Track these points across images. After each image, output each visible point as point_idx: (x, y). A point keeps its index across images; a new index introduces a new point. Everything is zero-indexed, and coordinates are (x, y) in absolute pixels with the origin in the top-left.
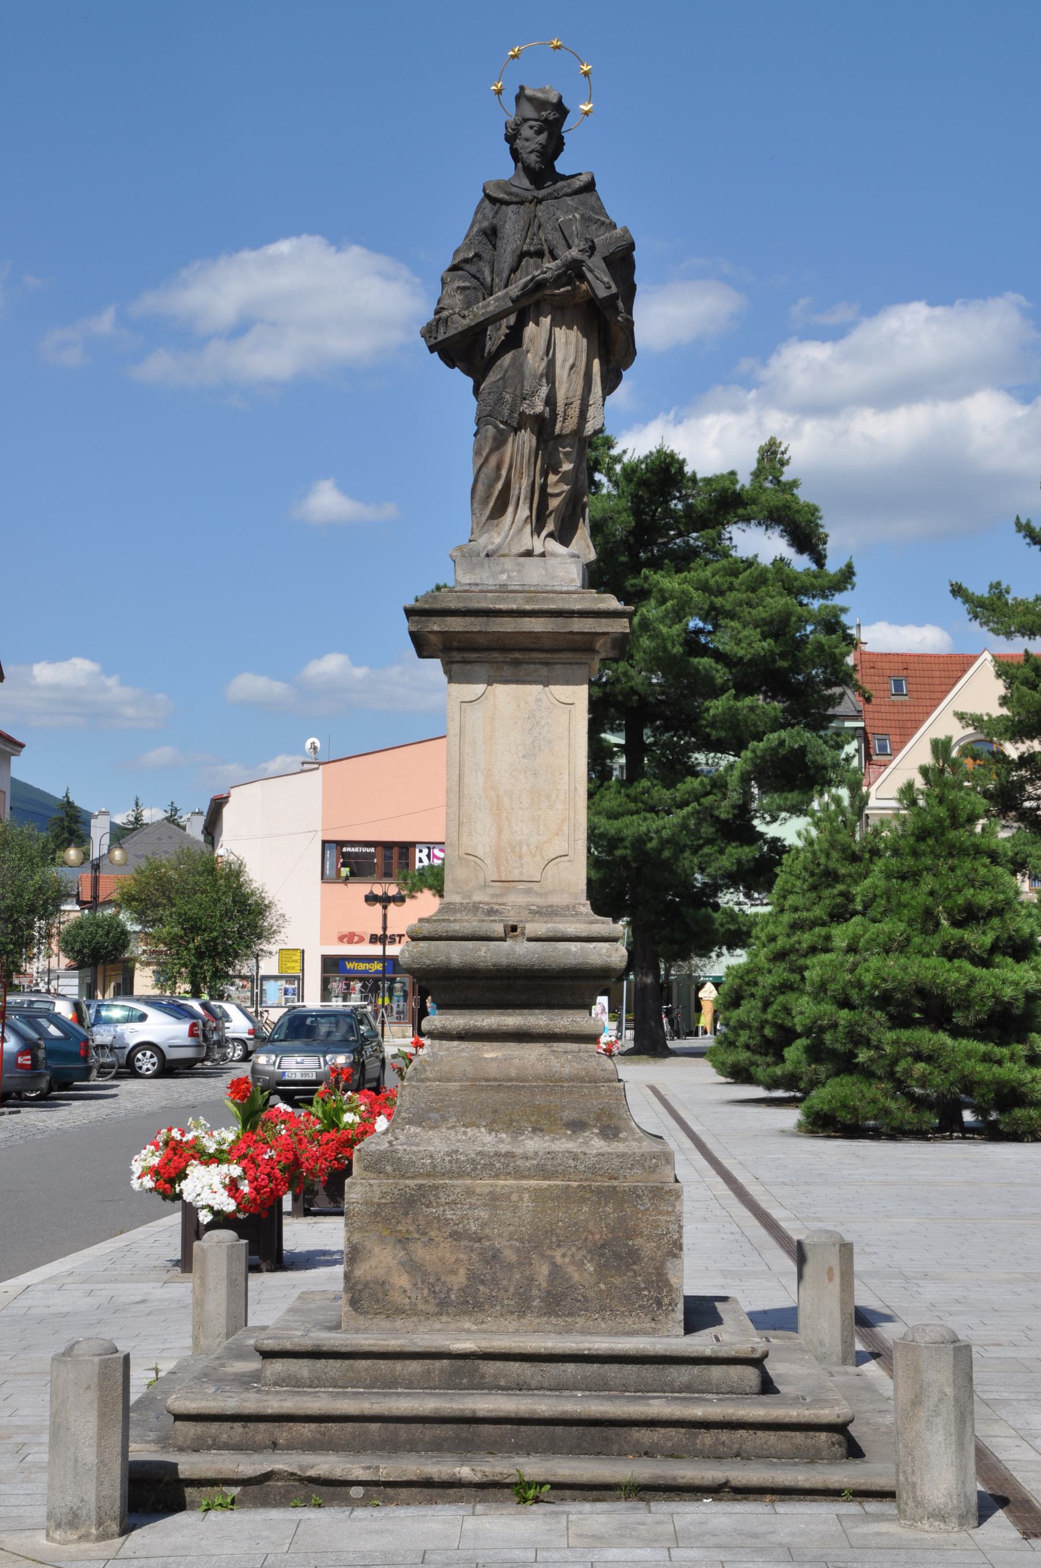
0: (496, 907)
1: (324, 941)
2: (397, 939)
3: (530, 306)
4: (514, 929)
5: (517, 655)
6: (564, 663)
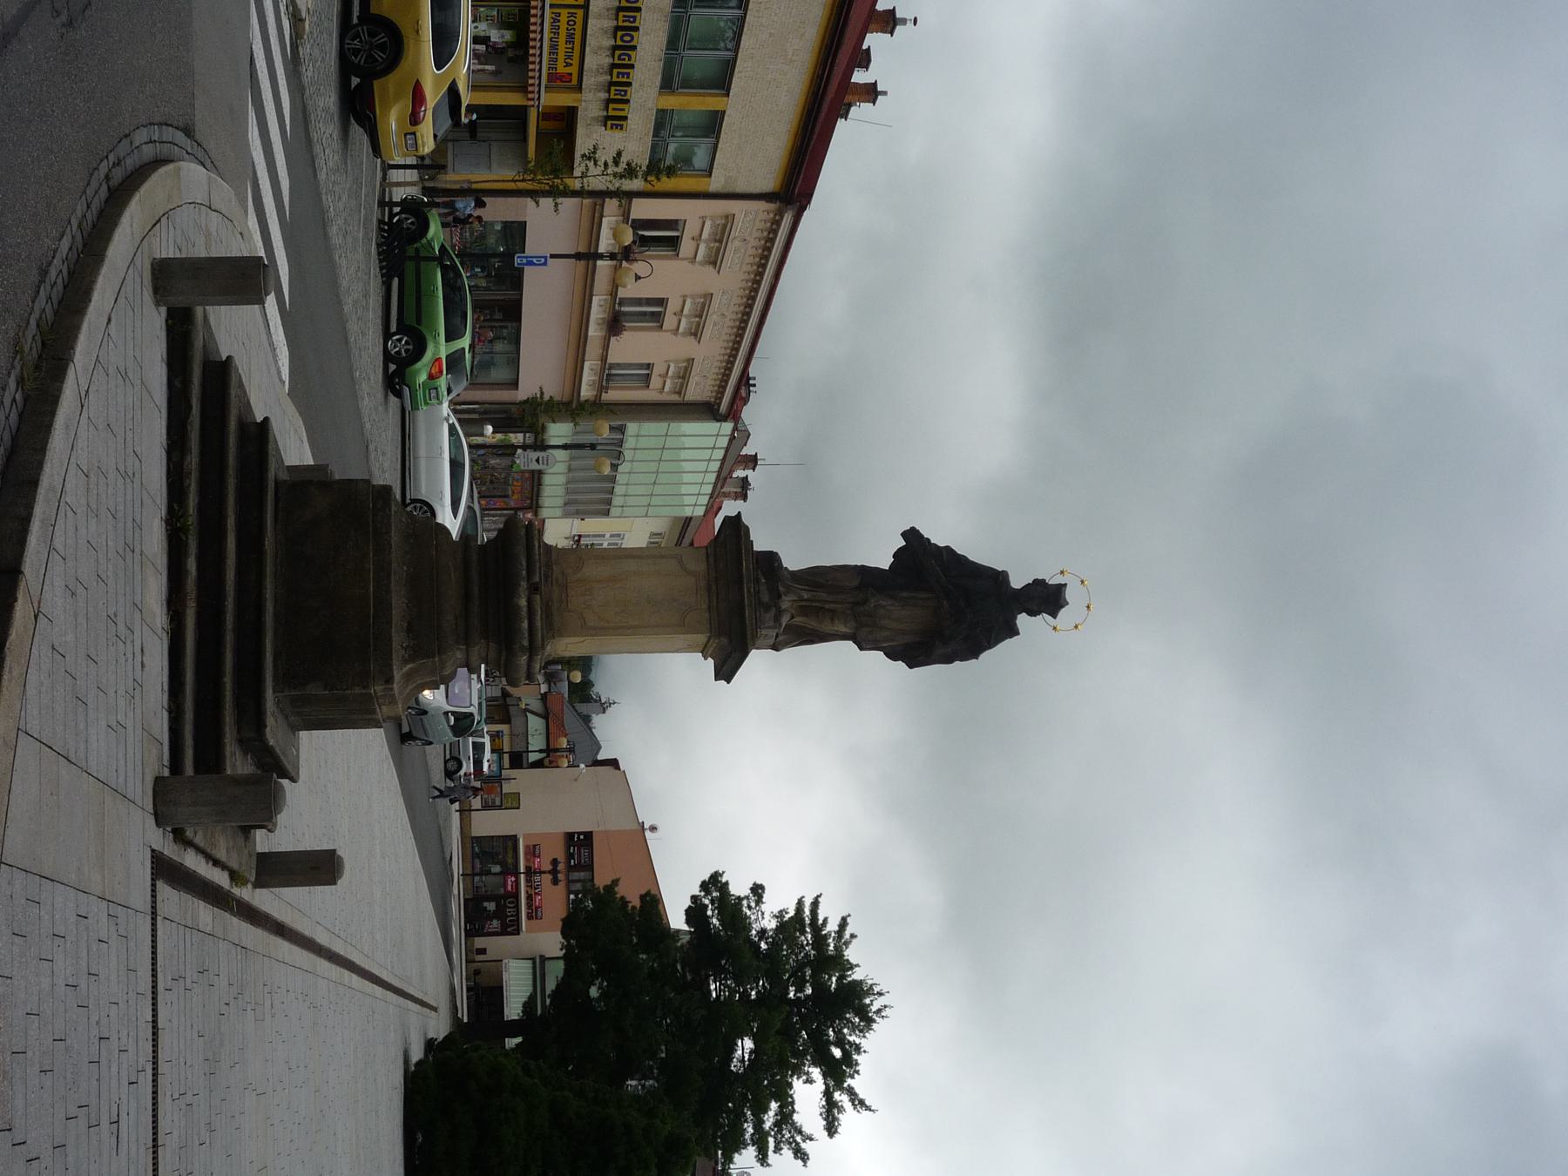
1: (525, 836)
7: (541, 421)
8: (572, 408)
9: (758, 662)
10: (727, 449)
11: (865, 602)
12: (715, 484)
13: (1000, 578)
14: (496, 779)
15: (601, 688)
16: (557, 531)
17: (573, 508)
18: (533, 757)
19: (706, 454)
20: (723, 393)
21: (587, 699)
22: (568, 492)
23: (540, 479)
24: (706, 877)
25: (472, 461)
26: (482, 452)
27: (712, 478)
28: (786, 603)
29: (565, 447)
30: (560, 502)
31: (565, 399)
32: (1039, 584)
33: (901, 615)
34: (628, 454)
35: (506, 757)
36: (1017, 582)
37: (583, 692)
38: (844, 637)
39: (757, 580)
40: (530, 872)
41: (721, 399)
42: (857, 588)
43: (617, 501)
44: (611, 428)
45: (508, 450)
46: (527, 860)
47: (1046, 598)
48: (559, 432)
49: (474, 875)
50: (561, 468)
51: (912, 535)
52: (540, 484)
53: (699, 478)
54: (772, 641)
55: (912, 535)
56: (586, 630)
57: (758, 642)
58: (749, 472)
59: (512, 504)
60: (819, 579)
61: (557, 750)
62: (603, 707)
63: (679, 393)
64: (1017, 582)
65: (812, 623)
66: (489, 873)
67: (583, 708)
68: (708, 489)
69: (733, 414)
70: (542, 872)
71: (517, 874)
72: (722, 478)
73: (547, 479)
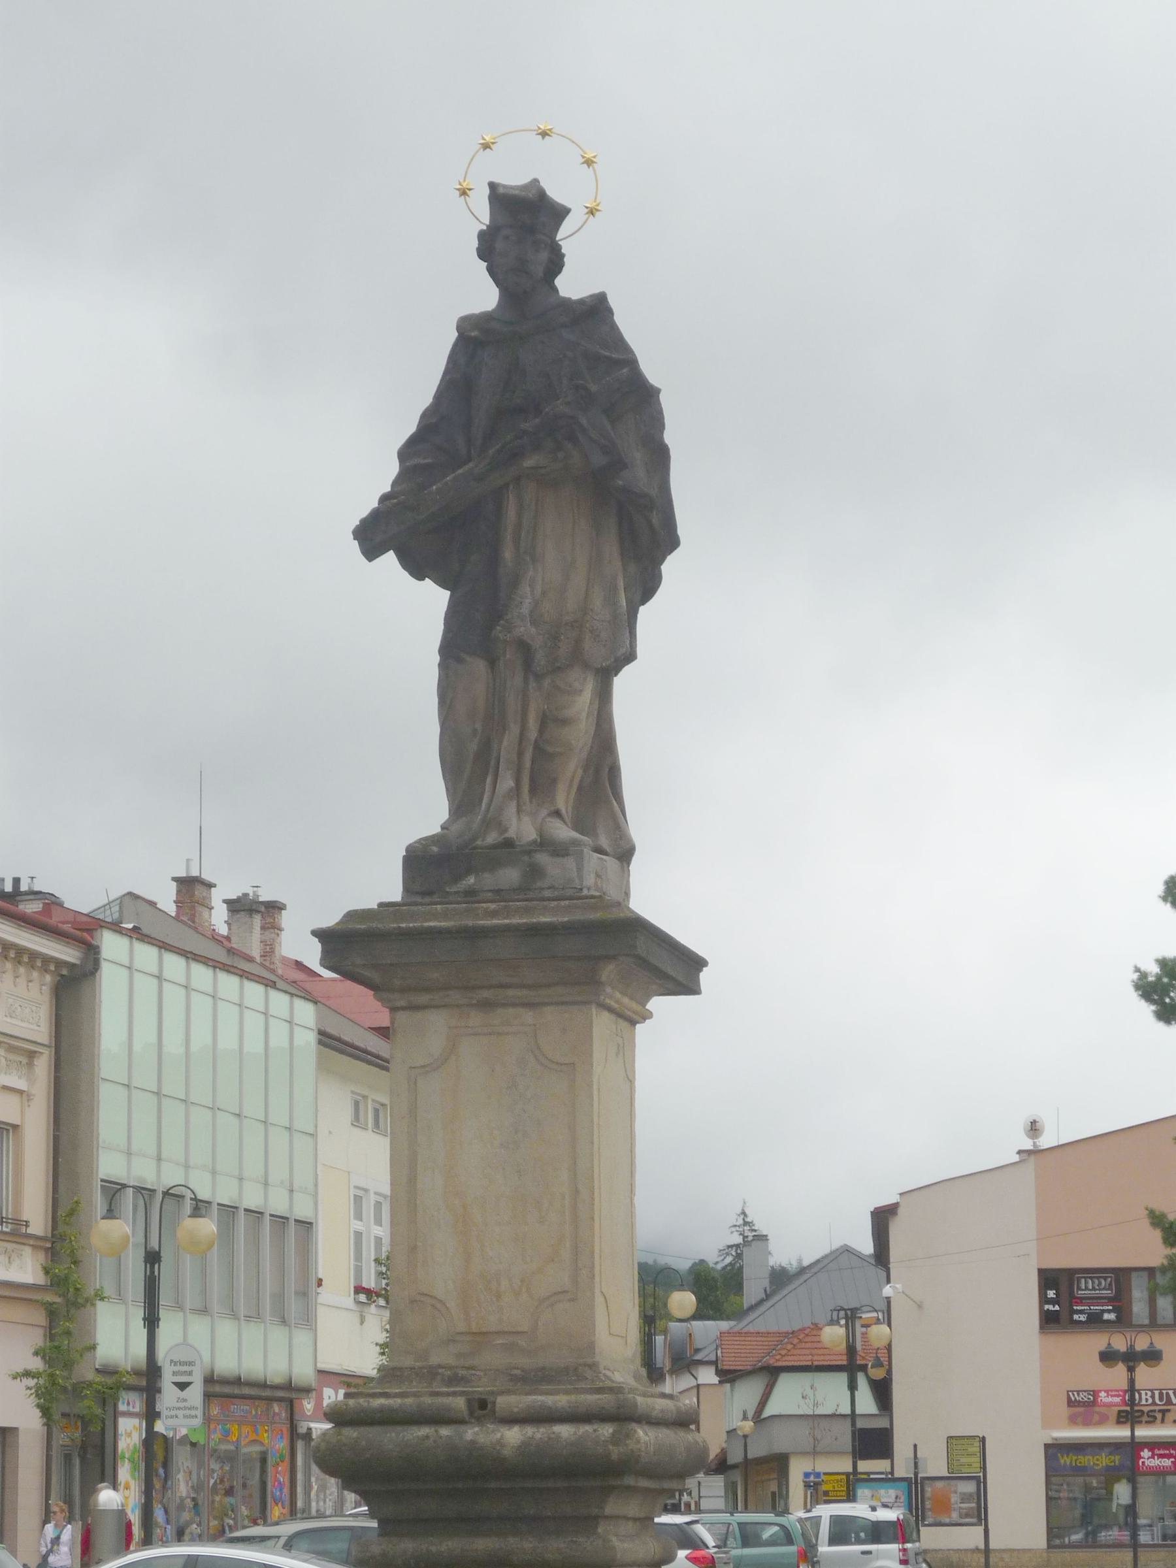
0: (462, 1372)
1: (1047, 1424)
2: (1159, 1416)
3: (507, 485)
4: (483, 1404)
5: (485, 994)
6: (557, 1004)
7: (90, 1376)
8: (62, 1304)
9: (657, 894)
10: (164, 946)
11: (524, 647)
12: (244, 975)
13: (475, 340)
14: (916, 1491)
15: (709, 1245)
16: (347, 1342)
17: (294, 1306)
18: (866, 1403)
19: (175, 996)
20: (34, 955)
21: (733, 1278)
22: (255, 1316)
23: (225, 1381)
24: (1147, 1010)
25: (180, 1536)
26: (159, 1515)
27: (229, 983)
28: (524, 829)
29: (152, 1322)
30: (278, 1334)
31: (40, 1318)
32: (487, 247)
33: (556, 560)
34: (171, 1177)
35: (864, 1466)
36: (485, 296)
37: (716, 1288)
38: (604, 695)
39: (471, 894)
40: (1130, 1416)
41: (47, 960)
42: (492, 663)
43: (278, 1204)
44: (110, 1214)
45: (157, 1454)
46: (1102, 1421)
47: (522, 229)
48: (115, 1336)
49: (1135, 1545)
50: (199, 1329)
51: (373, 536)
52: (238, 1381)
53: (228, 1013)
54: (611, 863)
55: (373, 536)
56: (578, 1289)
57: (613, 894)
58: (217, 898)
59: (282, 1445)
60: (468, 759)
61: (851, 1350)
62: (753, 1239)
63: (32, 1055)
64: (485, 296)
65: (571, 771)
66: (1131, 1510)
67: (753, 1290)
68: (255, 992)
69: (83, 932)
70: (1132, 1388)
71: (1134, 1447)
72: (229, 960)
73: (226, 1364)
